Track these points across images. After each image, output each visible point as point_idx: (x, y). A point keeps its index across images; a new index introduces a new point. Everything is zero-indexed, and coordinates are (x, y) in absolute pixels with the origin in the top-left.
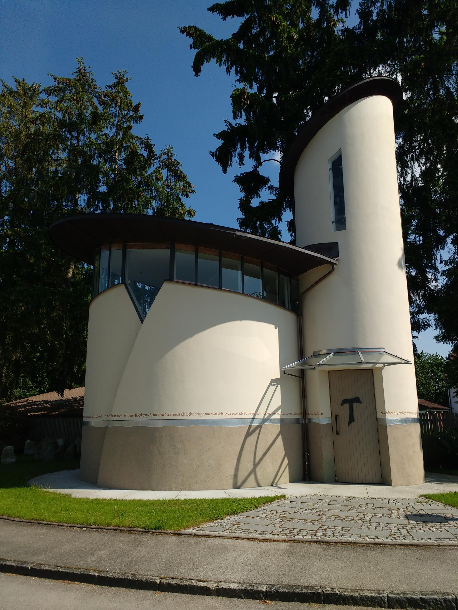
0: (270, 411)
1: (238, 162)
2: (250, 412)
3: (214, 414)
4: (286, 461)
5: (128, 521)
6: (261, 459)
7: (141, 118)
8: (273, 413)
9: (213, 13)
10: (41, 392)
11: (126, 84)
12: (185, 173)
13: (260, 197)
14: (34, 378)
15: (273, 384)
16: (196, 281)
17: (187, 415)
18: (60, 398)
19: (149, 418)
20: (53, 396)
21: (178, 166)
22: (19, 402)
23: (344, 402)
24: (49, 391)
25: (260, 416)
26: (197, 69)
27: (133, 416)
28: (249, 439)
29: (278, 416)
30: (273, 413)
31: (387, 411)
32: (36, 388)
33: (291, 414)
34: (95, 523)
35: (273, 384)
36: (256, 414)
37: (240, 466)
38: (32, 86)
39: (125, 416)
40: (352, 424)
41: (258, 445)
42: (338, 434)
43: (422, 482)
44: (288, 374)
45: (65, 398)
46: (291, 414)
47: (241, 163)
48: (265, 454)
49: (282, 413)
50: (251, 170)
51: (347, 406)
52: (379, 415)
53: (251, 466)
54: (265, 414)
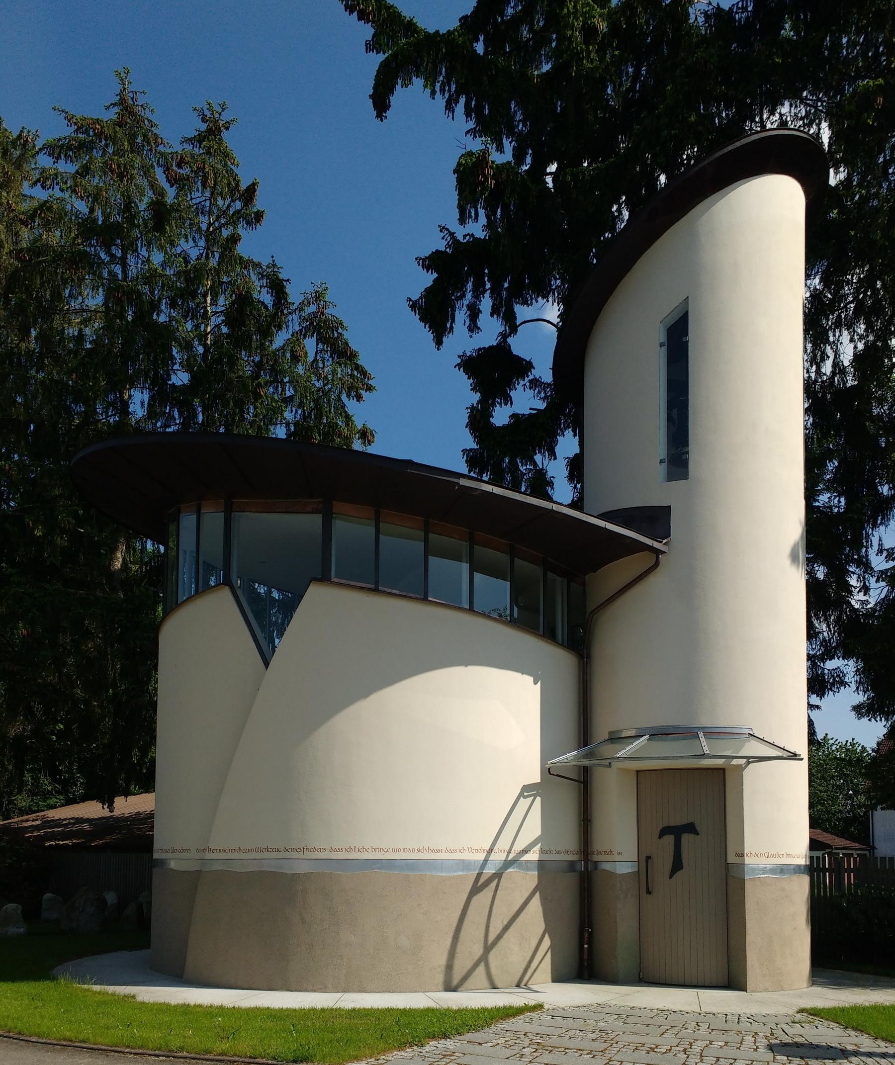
0: (519, 846)
1: (468, 323)
2: (479, 848)
3: (410, 851)
4: (547, 942)
6: (499, 937)
7: (259, 216)
8: (525, 851)
10: (69, 802)
13: (511, 404)
15: (525, 794)
16: (377, 583)
17: (357, 850)
19: (283, 855)
20: (93, 810)
21: (340, 330)
23: (665, 831)
24: (84, 799)
25: (499, 856)
26: (381, 103)
27: (250, 850)
28: (476, 899)
29: (533, 856)
30: (525, 851)
31: (746, 851)
32: (59, 793)
33: (559, 853)
34: (182, 1049)
35: (525, 794)
36: (490, 851)
37: (458, 950)
38: (19, 137)
39: (236, 850)
40: (679, 873)
41: (494, 911)
43: (805, 985)
44: (558, 775)
45: (117, 813)
46: (559, 853)
47: (473, 327)
48: (506, 928)
49: (542, 852)
51: (670, 839)
52: (732, 859)
53: (478, 951)
54: (509, 852)
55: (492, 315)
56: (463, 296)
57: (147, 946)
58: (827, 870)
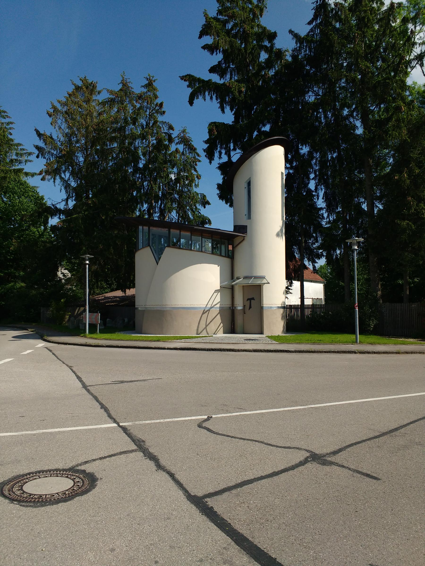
0: (214, 304)
1: (218, 157)
4: (222, 325)
5: (150, 339)
6: (209, 323)
7: (164, 112)
8: (216, 305)
9: (204, 50)
10: (112, 290)
11: (154, 84)
12: (195, 146)
14: (106, 282)
18: (124, 295)
19: (162, 306)
20: (119, 293)
21: (191, 142)
22: (100, 297)
23: (248, 299)
24: (116, 290)
25: (209, 306)
26: (191, 103)
30: (216, 305)
32: (109, 288)
33: (225, 305)
34: (139, 340)
36: (207, 305)
38: (92, 83)
42: (245, 313)
45: (127, 294)
46: (225, 305)
47: (220, 158)
48: (211, 322)
49: (220, 305)
50: (227, 160)
53: (204, 326)
55: (225, 154)
56: (217, 149)
57: (135, 330)
58: (318, 308)
